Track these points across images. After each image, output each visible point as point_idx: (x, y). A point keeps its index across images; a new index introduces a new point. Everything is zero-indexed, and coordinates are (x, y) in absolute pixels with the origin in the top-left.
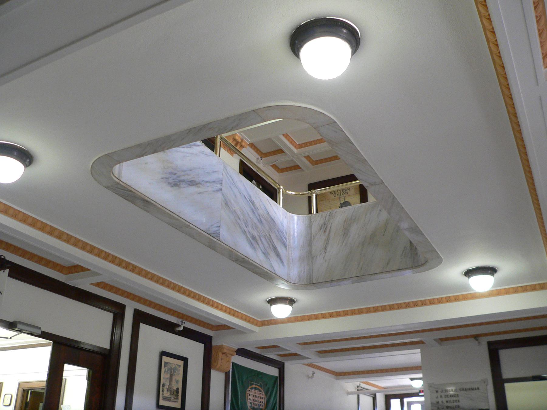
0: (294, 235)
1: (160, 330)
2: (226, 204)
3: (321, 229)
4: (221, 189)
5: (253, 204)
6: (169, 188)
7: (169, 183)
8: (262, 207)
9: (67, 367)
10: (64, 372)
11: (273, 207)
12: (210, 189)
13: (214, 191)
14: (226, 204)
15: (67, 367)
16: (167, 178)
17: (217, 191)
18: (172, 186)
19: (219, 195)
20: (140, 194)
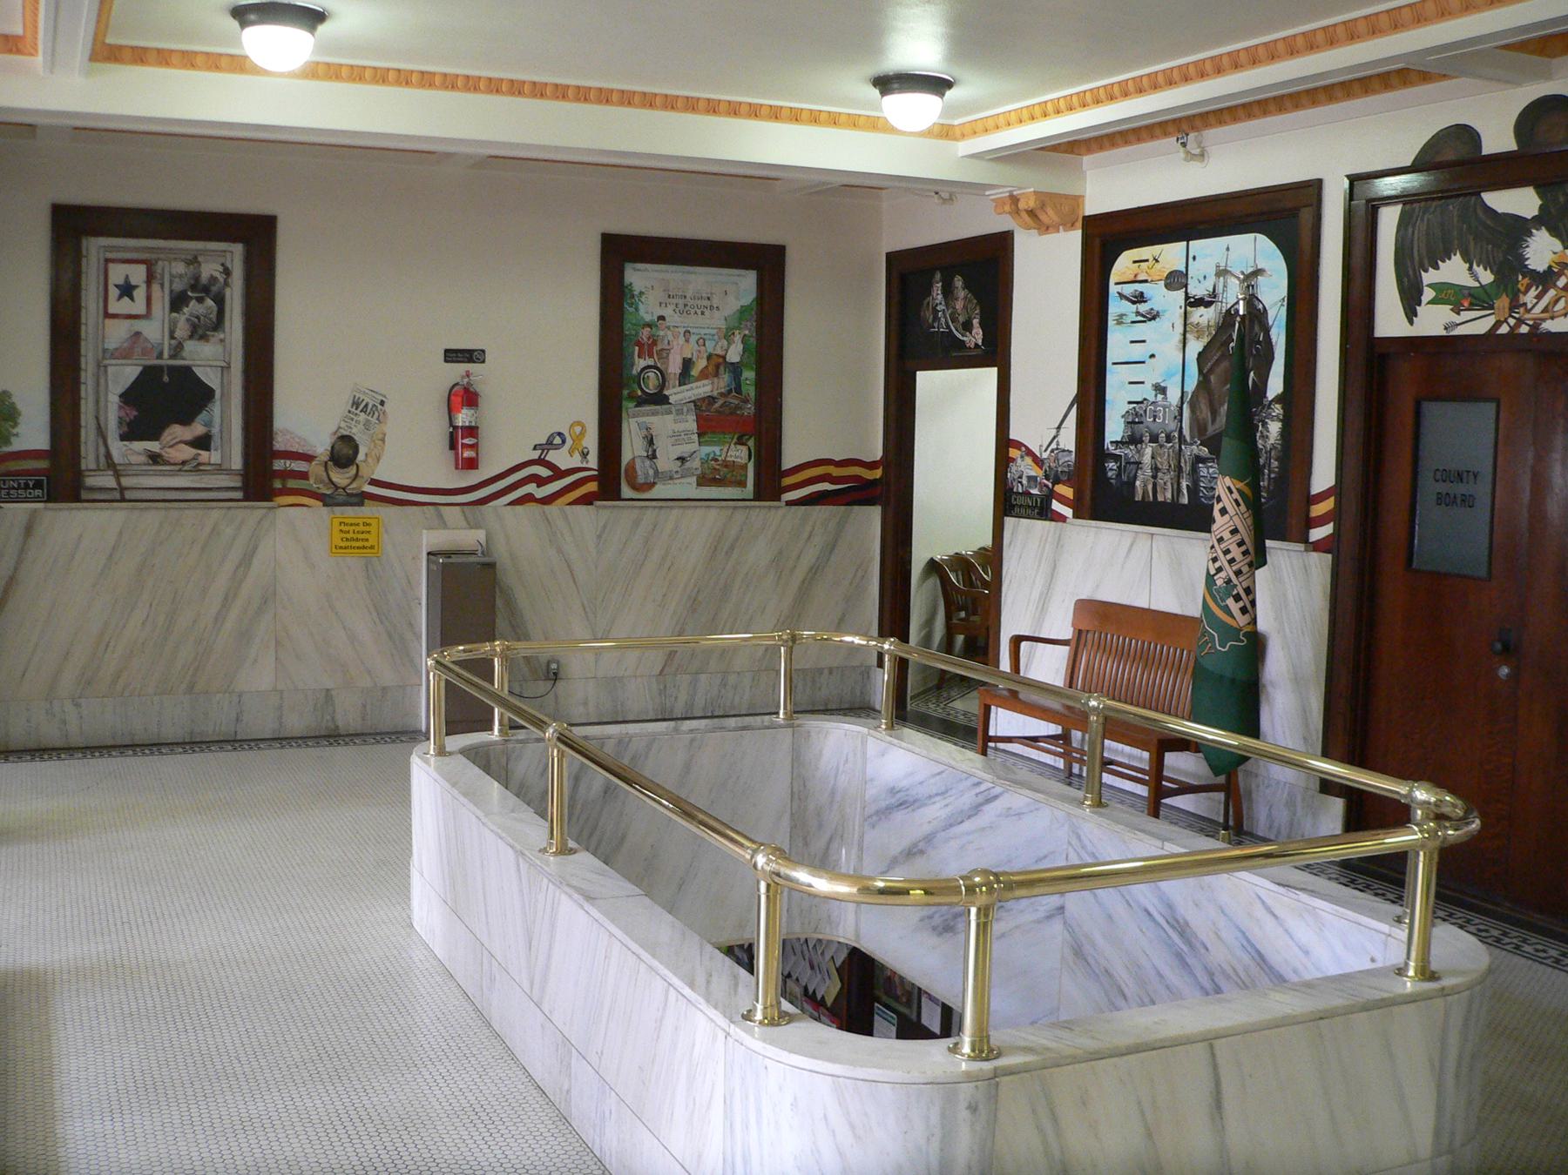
0: (1246, 969)
1: (711, 238)
2: (1078, 952)
3: (736, 985)
4: (1061, 909)
5: (1182, 934)
6: (934, 940)
7: (934, 929)
8: (1229, 935)
9: (995, 369)
10: (1153, 607)
11: (1293, 923)
12: (1028, 917)
13: (1039, 922)
14: (1078, 952)
15: (995, 369)
16: (930, 917)
17: (1049, 917)
18: (940, 934)
19: (1057, 927)
20: (1454, 1039)
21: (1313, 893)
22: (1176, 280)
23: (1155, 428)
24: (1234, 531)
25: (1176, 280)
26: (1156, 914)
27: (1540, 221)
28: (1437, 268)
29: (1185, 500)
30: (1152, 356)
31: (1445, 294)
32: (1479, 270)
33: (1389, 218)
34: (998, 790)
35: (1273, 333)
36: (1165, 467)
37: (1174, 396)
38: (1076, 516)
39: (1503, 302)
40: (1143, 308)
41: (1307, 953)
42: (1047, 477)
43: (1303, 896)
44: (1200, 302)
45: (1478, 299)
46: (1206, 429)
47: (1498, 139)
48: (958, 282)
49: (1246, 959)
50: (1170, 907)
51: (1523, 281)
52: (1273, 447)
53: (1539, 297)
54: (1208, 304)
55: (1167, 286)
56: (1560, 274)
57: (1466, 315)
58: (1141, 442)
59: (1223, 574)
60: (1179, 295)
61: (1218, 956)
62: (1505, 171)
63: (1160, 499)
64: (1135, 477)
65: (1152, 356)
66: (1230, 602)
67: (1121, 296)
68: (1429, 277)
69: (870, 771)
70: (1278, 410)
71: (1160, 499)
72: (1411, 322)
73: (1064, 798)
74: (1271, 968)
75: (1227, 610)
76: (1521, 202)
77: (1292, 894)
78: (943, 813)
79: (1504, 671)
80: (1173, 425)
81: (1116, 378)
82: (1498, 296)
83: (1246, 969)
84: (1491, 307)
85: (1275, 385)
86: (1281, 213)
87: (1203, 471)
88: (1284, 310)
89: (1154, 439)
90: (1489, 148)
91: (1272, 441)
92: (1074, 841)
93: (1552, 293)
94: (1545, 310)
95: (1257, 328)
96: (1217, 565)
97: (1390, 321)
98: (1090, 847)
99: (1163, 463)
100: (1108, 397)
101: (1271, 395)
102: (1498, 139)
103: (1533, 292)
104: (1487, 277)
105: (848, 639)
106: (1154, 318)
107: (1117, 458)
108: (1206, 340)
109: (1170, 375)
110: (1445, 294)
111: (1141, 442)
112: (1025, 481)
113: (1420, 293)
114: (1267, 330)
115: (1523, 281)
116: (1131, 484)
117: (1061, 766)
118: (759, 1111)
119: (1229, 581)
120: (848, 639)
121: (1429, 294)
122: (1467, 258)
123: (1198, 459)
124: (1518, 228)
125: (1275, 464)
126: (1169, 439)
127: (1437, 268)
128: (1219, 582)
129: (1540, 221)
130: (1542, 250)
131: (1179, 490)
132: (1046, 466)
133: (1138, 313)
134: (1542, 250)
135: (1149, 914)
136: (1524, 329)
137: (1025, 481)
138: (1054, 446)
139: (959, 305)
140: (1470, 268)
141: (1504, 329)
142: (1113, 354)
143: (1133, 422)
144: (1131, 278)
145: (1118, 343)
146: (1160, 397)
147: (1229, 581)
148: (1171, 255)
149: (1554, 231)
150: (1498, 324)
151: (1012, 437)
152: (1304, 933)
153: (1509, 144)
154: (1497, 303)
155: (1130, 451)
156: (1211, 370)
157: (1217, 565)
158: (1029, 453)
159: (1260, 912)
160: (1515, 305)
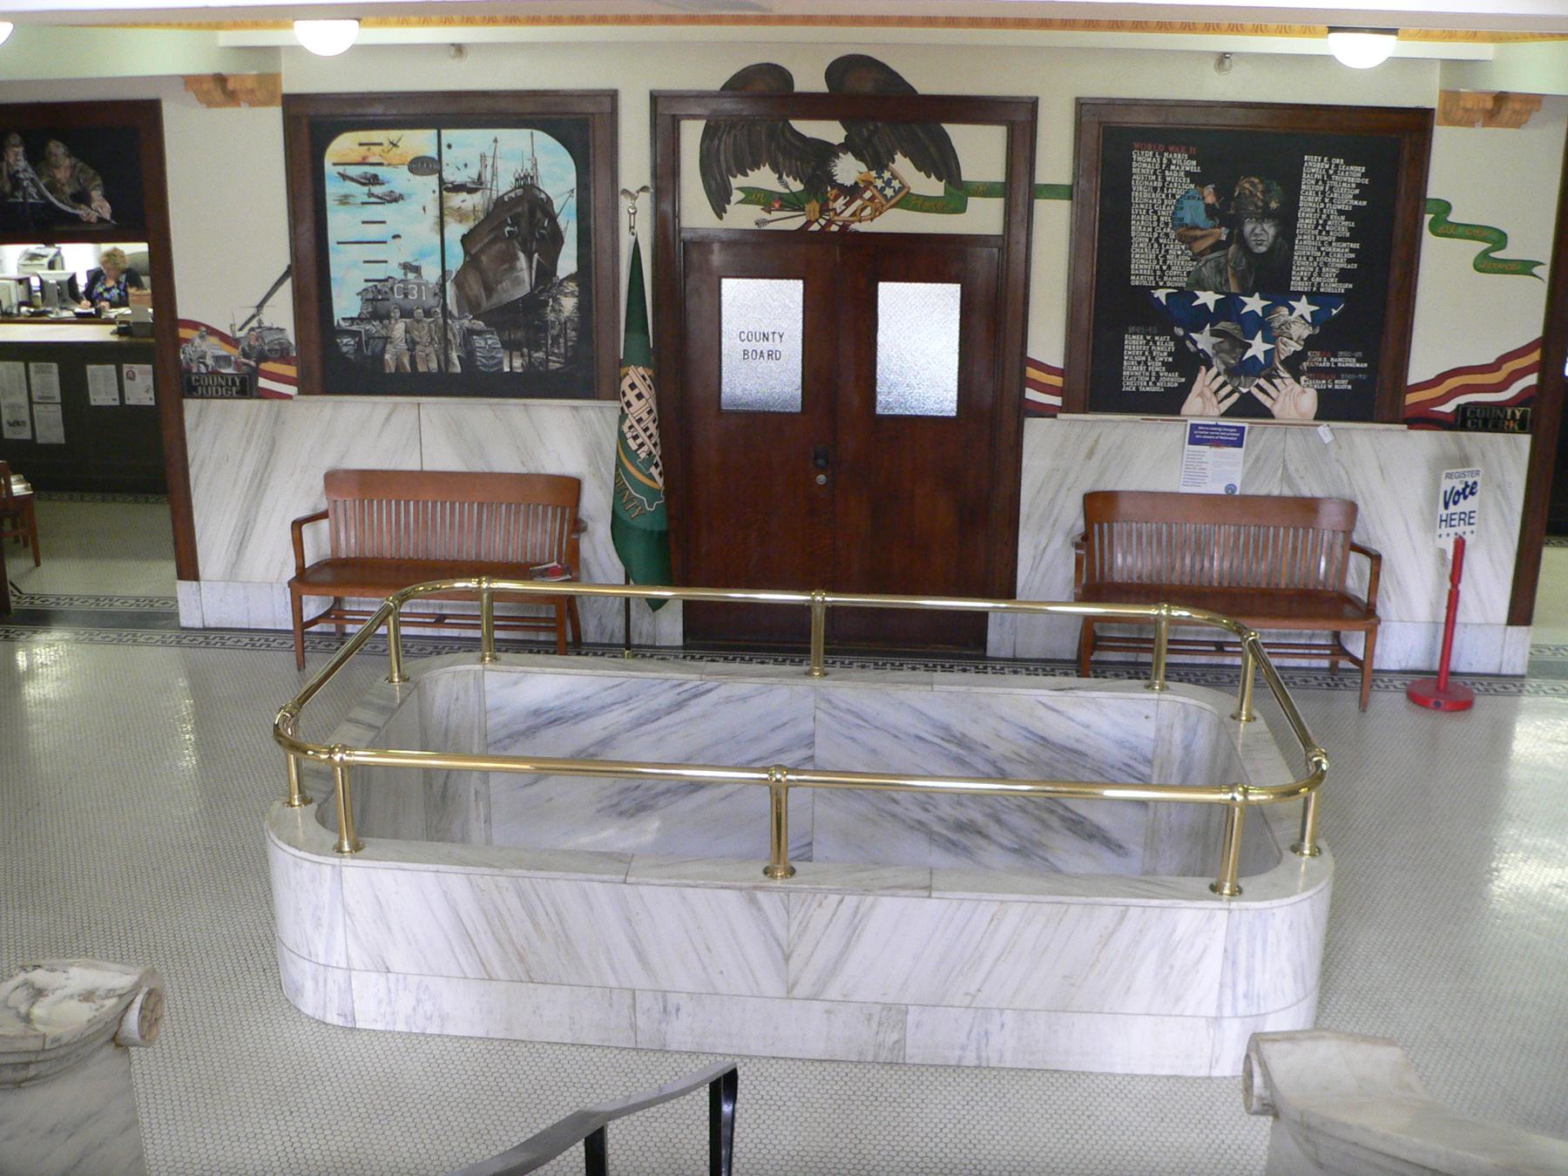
8: (1004, 730)
11: (1072, 712)
21: (1087, 689)
22: (420, 165)
23: (407, 305)
24: (650, 412)
25: (420, 165)
26: (930, 738)
27: (846, 147)
28: (746, 175)
29: (457, 368)
30: (396, 237)
31: (753, 196)
32: (790, 180)
33: (692, 134)
34: (709, 685)
35: (561, 221)
36: (426, 339)
37: (431, 274)
38: (305, 390)
39: (813, 207)
40: (377, 190)
41: (1088, 727)
42: (245, 355)
43: (1081, 693)
44: (459, 188)
45: (790, 203)
46: (479, 305)
47: (810, 79)
48: (57, 149)
49: (1029, 744)
50: (946, 728)
51: (831, 192)
52: (569, 319)
53: (847, 205)
54: (471, 191)
55: (411, 170)
56: (866, 189)
57: (775, 215)
58: (389, 317)
59: (645, 448)
60: (432, 181)
61: (999, 749)
62: (814, 106)
63: (421, 368)
64: (383, 350)
65: (396, 237)
66: (653, 470)
67: (344, 177)
68: (737, 182)
69: (490, 702)
70: (572, 287)
71: (421, 368)
72: (721, 218)
73: (798, 675)
74: (1054, 744)
75: (651, 477)
76: (831, 131)
77: (1070, 693)
78: (626, 717)
79: (821, 479)
80: (432, 302)
81: (339, 260)
82: (808, 202)
83: (1029, 751)
84: (803, 210)
85: (567, 263)
86: (579, 123)
87: (479, 342)
88: (573, 202)
89: (406, 313)
90: (799, 87)
91: (566, 314)
92: (823, 705)
93: (858, 203)
94: (853, 215)
95: (539, 215)
96: (639, 441)
97: (696, 212)
98: (843, 705)
99: (422, 334)
100: (333, 275)
101: (562, 273)
102: (810, 79)
103: (841, 201)
104: (797, 186)
105: (457, 585)
106: (395, 200)
107: (353, 334)
108: (471, 224)
109: (423, 255)
110: (753, 196)
111: (389, 317)
112: (210, 362)
113: (729, 194)
114: (553, 218)
115: (831, 192)
116: (379, 358)
117: (333, 629)
118: (1265, 942)
119: (650, 453)
120: (457, 585)
121: (737, 196)
122: (775, 168)
123: (471, 332)
124: (827, 152)
125: (572, 334)
126: (428, 313)
127: (746, 175)
128: (643, 456)
129: (846, 147)
130: (848, 169)
131: (448, 361)
132: (244, 344)
133: (371, 195)
134: (848, 169)
135: (920, 738)
136: (834, 228)
137: (210, 362)
138: (254, 324)
139: (62, 175)
140: (780, 178)
141: (815, 227)
142: (333, 235)
143: (374, 299)
144: (359, 159)
145: (340, 223)
146: (411, 276)
147: (650, 453)
148: (420, 141)
149: (859, 156)
150: (809, 223)
151: (180, 316)
152: (1083, 715)
153: (822, 87)
154: (807, 207)
155: (374, 327)
156: (482, 251)
157: (639, 441)
158: (212, 331)
159: (1041, 711)
160: (824, 209)
